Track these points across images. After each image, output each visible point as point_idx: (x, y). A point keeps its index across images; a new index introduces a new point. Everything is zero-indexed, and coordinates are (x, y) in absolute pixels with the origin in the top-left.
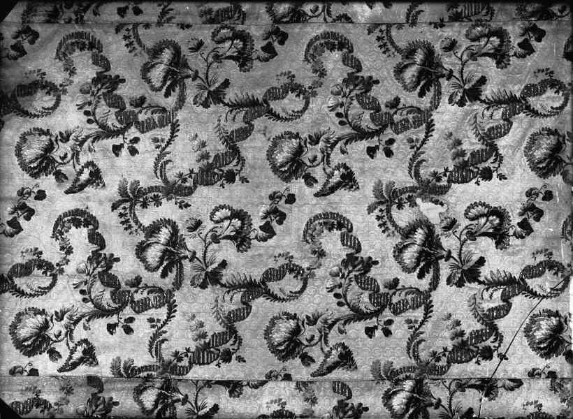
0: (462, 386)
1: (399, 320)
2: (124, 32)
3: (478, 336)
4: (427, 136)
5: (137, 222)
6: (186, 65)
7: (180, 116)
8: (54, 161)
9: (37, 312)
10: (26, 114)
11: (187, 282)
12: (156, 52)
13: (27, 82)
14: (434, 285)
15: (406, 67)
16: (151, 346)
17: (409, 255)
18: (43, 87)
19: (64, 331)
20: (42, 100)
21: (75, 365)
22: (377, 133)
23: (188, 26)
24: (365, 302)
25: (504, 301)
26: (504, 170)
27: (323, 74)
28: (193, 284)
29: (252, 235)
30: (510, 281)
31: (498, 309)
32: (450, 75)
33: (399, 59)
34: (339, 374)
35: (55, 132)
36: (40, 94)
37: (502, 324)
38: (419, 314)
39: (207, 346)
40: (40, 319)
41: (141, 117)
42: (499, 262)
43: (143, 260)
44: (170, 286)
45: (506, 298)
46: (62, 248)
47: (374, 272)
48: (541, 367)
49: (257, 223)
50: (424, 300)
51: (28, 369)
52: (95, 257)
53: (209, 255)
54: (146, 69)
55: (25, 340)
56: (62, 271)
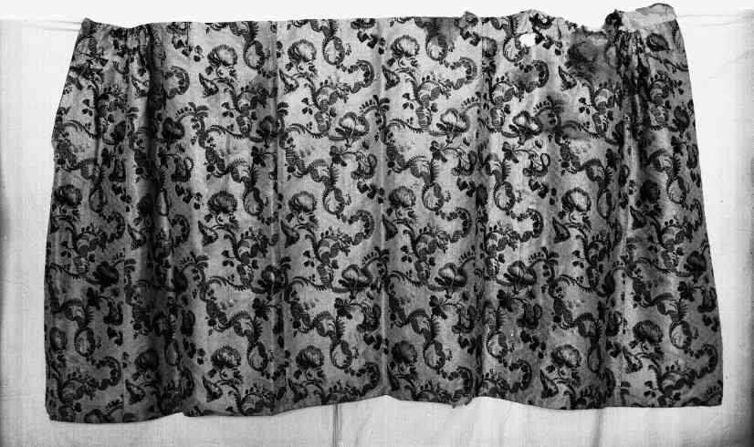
0: (279, 312)
1: (315, 270)
2: (476, 97)
3: (307, 318)
4: (413, 282)
5: (367, 111)
6: (455, 136)
7: (425, 134)
8: (299, 63)
9: (314, 55)
10: (428, 40)
11: (333, 143)
12: (464, 118)
13: (447, 41)
14: (336, 290)
15: (453, 270)
16: (296, 125)
17: (352, 274)
18: (444, 51)
19: (303, 72)
20: (436, 49)
21: (283, 80)
22: (415, 252)
23: (477, 137)
24: (324, 249)
25: (245, 332)
26: (215, 334)
27: (520, 219)
28: (332, 147)
29: (361, 180)
30: (339, 334)
31: (323, 329)
32: (352, 297)
33: (458, 265)
34: (283, 237)
35: (315, 63)
36: (440, 49)
37: (314, 332)
38: (318, 282)
39: (297, 158)
40: (310, 57)
41: (324, 116)
42: (350, 326)
43: (345, 117)
44: (330, 134)
45: (329, 333)
46: (352, 67)
47: (341, 253)
48: (130, 360)
49: (368, 182)
50: (327, 284)
51: (281, 52)
52: (449, 84)
53: (450, 151)
54: (454, 112)
55: (297, 49)
56: (338, 67)
